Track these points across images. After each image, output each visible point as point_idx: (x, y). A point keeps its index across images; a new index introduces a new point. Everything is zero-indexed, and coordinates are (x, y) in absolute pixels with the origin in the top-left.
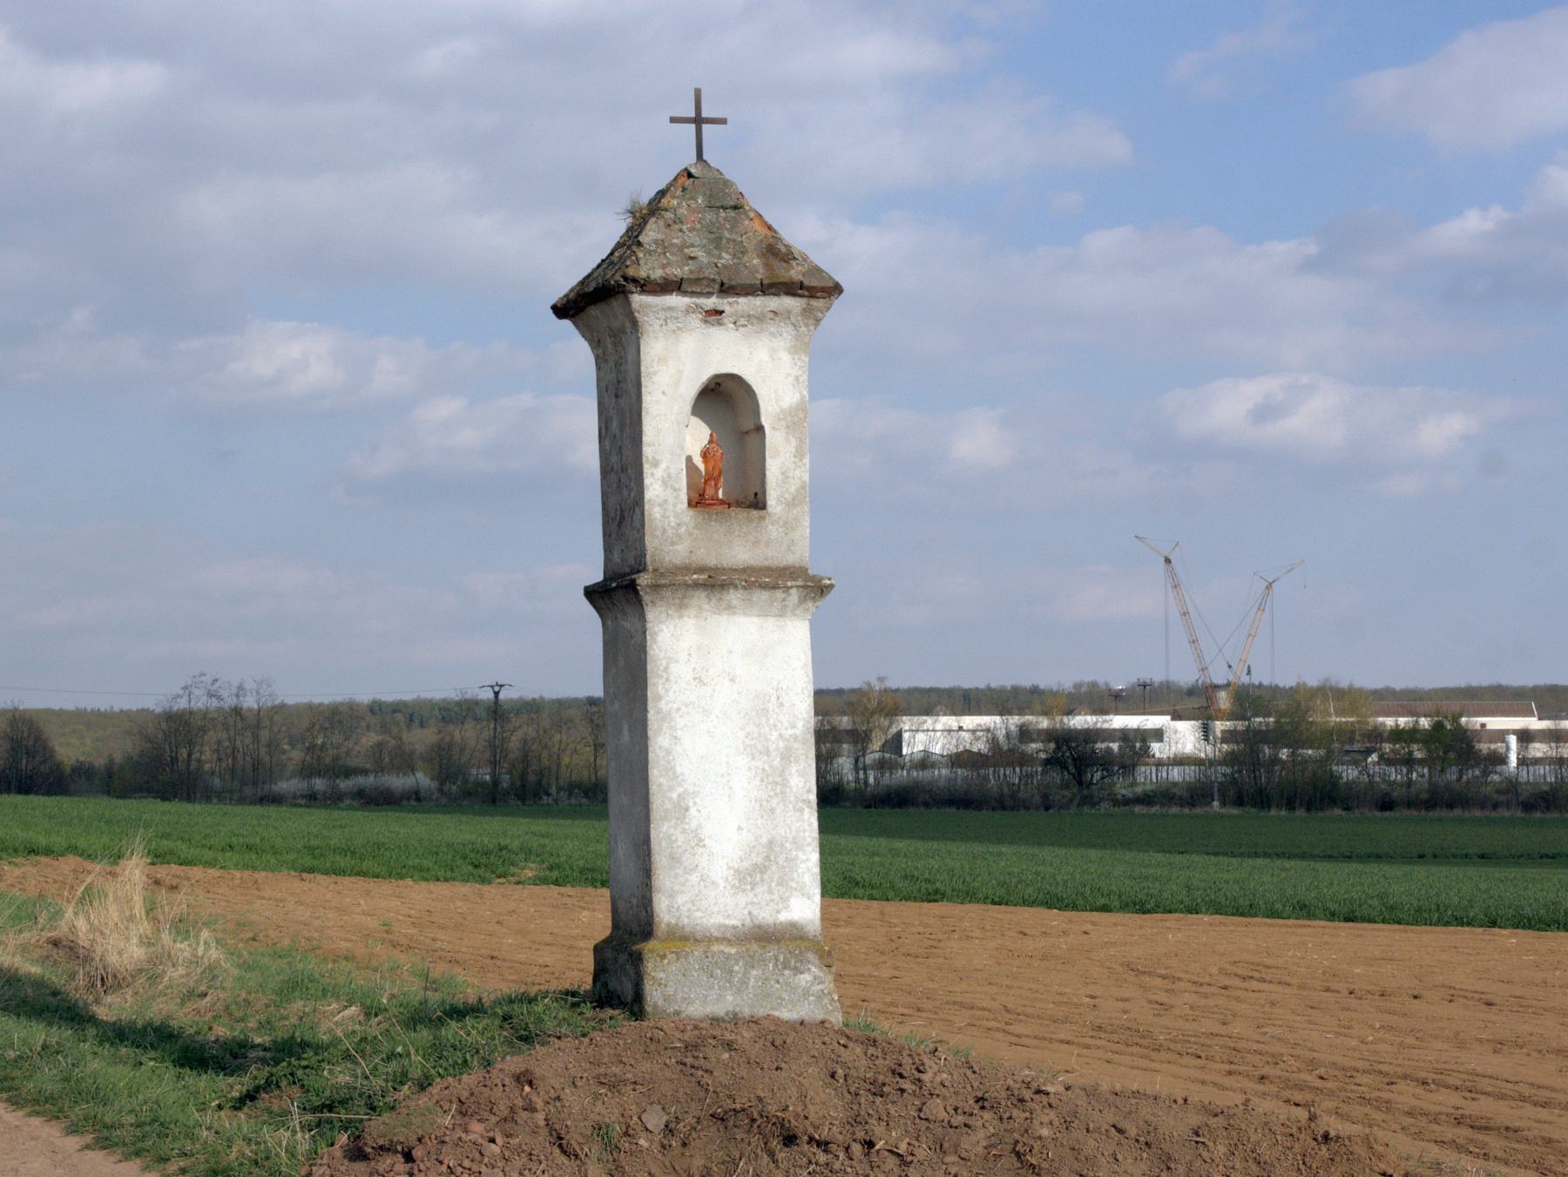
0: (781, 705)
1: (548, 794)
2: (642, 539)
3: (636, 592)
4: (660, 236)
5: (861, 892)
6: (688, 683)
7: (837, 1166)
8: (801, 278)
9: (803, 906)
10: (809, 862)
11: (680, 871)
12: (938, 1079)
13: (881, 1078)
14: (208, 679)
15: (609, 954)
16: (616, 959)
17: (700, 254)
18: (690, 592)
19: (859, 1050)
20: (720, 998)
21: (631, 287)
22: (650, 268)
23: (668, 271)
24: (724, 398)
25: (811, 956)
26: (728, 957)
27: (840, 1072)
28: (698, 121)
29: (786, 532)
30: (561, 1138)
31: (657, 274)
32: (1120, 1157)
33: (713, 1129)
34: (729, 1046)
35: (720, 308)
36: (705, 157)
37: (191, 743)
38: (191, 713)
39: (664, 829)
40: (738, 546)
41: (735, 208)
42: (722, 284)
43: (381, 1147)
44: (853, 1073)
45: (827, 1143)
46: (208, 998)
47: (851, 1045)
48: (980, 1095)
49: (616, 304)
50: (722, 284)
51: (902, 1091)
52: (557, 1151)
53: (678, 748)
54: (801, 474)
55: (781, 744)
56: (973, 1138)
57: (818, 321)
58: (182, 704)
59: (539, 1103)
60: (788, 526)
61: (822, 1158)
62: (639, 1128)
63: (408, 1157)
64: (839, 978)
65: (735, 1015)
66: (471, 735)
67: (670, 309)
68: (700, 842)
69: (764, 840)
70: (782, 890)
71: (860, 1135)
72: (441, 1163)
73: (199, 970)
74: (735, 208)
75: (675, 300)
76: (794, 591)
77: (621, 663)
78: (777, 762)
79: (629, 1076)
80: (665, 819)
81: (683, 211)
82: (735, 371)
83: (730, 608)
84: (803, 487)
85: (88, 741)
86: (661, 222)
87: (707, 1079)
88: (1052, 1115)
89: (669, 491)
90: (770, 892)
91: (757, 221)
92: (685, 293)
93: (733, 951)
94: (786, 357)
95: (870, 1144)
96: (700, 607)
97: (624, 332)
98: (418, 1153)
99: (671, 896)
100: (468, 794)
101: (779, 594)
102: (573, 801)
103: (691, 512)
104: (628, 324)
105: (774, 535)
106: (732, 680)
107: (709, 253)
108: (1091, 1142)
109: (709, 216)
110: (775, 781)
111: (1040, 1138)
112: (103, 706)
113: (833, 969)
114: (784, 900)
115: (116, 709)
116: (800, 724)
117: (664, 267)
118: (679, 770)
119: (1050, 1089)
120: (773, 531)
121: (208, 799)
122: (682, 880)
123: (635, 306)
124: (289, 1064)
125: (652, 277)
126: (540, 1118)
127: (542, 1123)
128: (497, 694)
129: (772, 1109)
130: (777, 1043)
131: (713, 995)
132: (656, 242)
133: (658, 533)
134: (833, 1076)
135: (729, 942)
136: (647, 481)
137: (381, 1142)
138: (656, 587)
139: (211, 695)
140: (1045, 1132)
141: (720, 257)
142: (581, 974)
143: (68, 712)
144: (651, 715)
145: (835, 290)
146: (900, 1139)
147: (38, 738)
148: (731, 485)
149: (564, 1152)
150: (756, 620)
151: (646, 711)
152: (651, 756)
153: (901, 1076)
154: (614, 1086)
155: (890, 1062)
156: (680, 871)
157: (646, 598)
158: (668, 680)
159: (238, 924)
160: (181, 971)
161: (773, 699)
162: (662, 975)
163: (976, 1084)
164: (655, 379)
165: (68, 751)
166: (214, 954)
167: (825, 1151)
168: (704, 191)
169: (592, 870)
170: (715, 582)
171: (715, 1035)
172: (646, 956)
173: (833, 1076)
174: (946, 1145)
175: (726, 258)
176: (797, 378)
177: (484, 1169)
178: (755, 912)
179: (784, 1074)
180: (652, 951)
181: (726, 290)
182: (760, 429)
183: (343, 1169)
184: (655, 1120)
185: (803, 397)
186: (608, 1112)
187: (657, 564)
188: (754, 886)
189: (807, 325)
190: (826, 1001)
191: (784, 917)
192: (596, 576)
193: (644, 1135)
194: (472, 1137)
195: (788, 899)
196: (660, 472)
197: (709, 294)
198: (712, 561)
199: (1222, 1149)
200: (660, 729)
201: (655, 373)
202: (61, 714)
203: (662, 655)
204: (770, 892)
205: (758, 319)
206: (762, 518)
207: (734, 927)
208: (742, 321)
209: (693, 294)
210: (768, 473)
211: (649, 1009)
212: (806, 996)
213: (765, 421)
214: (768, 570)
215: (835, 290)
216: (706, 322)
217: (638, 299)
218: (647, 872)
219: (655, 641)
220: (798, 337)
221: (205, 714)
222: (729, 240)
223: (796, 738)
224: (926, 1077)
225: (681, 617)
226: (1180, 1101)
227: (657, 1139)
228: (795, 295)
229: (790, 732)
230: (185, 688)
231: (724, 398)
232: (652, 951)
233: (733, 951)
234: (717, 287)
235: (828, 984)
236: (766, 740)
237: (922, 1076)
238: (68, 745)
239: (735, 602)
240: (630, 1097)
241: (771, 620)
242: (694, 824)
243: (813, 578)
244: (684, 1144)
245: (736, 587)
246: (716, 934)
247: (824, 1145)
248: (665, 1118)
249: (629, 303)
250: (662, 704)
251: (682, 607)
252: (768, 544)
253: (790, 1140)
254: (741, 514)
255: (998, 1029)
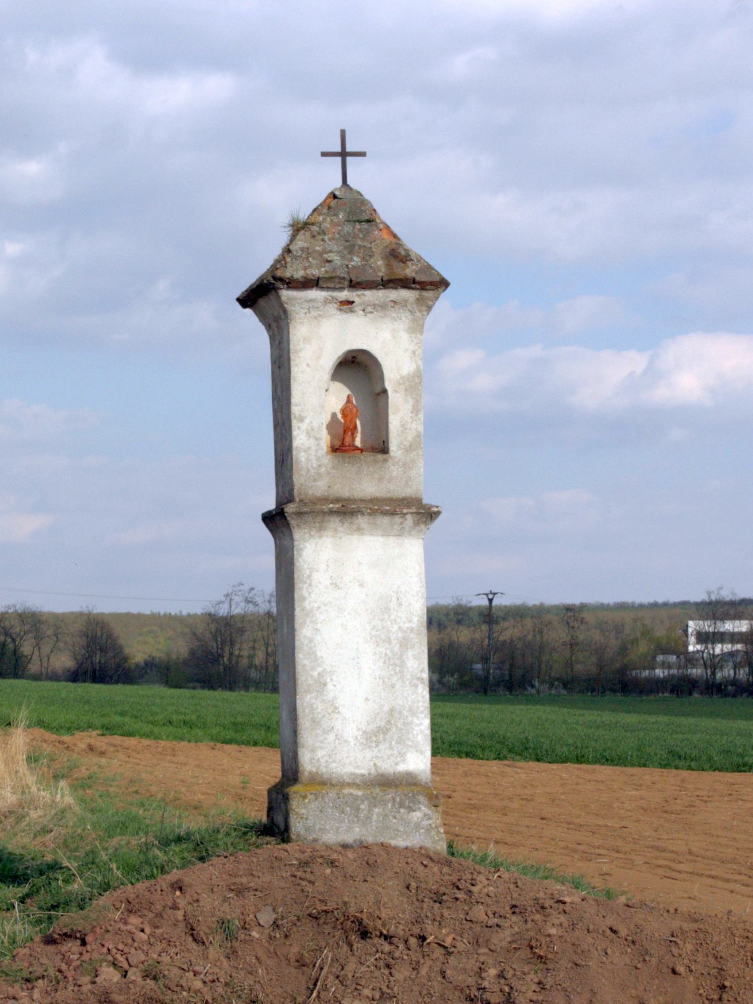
0: (400, 604)
1: (533, 686)
2: (291, 478)
3: (285, 518)
4: (305, 245)
5: (682, 763)
6: (326, 587)
7: (397, 954)
8: (413, 275)
9: (418, 760)
10: (421, 727)
11: (319, 732)
12: (486, 890)
13: (443, 889)
14: (246, 588)
15: (274, 796)
16: (277, 799)
17: (336, 259)
18: (327, 518)
19: (436, 869)
20: (350, 829)
21: (279, 284)
22: (295, 271)
23: (308, 272)
24: (356, 366)
25: (421, 798)
26: (356, 798)
27: (413, 884)
28: (344, 154)
29: (408, 468)
30: (193, 929)
31: (299, 274)
32: (609, 951)
33: (308, 926)
34: (332, 863)
35: (351, 299)
36: (349, 182)
37: (232, 643)
38: (232, 616)
39: (307, 699)
40: (365, 483)
41: (368, 221)
42: (351, 281)
43: (65, 934)
44: (423, 885)
45: (391, 937)
46: (52, 834)
47: (431, 864)
48: (514, 903)
49: (272, 296)
50: (351, 281)
51: (457, 899)
52: (190, 939)
53: (318, 638)
54: (417, 426)
55: (400, 635)
56: (501, 935)
57: (429, 308)
58: (223, 611)
59: (182, 903)
60: (407, 466)
61: (387, 948)
62: (253, 923)
63: (84, 943)
64: (445, 813)
65: (361, 842)
66: (558, 635)
67: (311, 300)
68: (336, 710)
69: (386, 709)
70: (400, 747)
71: (416, 930)
72: (103, 946)
73: (53, 812)
74: (368, 221)
75: (315, 294)
76: (409, 517)
77: (283, 572)
78: (397, 649)
79: (252, 885)
80: (308, 691)
81: (327, 225)
82: (364, 347)
83: (359, 530)
84: (418, 436)
85: (161, 640)
86: (308, 234)
87: (309, 889)
88: (563, 918)
89: (312, 441)
90: (391, 748)
91: (385, 231)
92: (322, 288)
93: (360, 793)
94: (404, 336)
95: (423, 938)
96: (336, 530)
97: (280, 318)
98: (89, 939)
99: (313, 751)
100: (463, 685)
101: (397, 519)
102: (553, 692)
103: (329, 457)
104: (282, 314)
105: (395, 473)
106: (362, 585)
107: (343, 257)
108: (591, 940)
109: (348, 228)
110: (395, 663)
111: (549, 936)
112: (173, 610)
113: (440, 809)
114: (402, 755)
115: (185, 613)
116: (415, 619)
117: (305, 269)
118: (319, 654)
119: (567, 899)
120: (394, 470)
121: (246, 688)
122: (321, 738)
123: (284, 299)
124: (48, 876)
125: (296, 276)
126: (180, 914)
127: (181, 918)
128: (491, 601)
129: (352, 910)
130: (371, 862)
131: (344, 827)
132: (302, 249)
133: (303, 472)
134: (408, 888)
135: (358, 786)
136: (295, 433)
137: (65, 931)
138: (299, 514)
139: (248, 601)
140: (553, 931)
141: (351, 260)
142: (258, 814)
143: (144, 615)
144: (298, 612)
145: (443, 284)
146: (447, 935)
147: (110, 636)
148: (361, 435)
149: (195, 940)
150: (381, 539)
151: (293, 609)
152: (297, 643)
153: (458, 888)
154: (240, 891)
155: (454, 878)
156: (319, 732)
157: (293, 523)
158: (310, 585)
159: (131, 781)
160: (40, 813)
161: (394, 599)
162: (304, 811)
163: (515, 896)
164: (301, 354)
165: (138, 651)
166: (69, 800)
167: (390, 943)
168: (348, 211)
169: (460, 743)
170: (346, 510)
171: (331, 858)
172: (292, 796)
173: (408, 888)
174: (481, 940)
175: (356, 260)
176: (414, 352)
177: (133, 951)
178: (379, 764)
179: (367, 884)
180: (296, 793)
181: (354, 285)
182: (385, 391)
183: (39, 950)
184: (266, 917)
185: (418, 367)
186: (232, 912)
187: (302, 497)
188: (378, 743)
189: (420, 311)
190: (433, 833)
191: (402, 768)
192: (270, 504)
193: (257, 928)
194: (129, 927)
195: (405, 754)
196: (304, 426)
197: (342, 289)
198: (345, 493)
199: (689, 947)
200: (305, 622)
201: (301, 350)
202: (138, 617)
203: (306, 566)
204: (391, 748)
205: (381, 307)
206: (386, 460)
207: (362, 775)
208: (369, 309)
209: (328, 289)
210: (390, 426)
211: (293, 837)
212: (418, 829)
213: (388, 385)
214: (390, 501)
215: (443, 284)
216: (341, 310)
217: (286, 294)
218: (295, 732)
219: (300, 556)
220: (415, 320)
221: (243, 617)
222: (360, 246)
223: (412, 630)
224: (475, 889)
225: (321, 537)
226: (672, 911)
227: (267, 931)
228: (409, 288)
229: (407, 625)
230: (227, 595)
231: (356, 366)
232: (296, 793)
233: (360, 793)
234: (346, 283)
235: (436, 819)
236: (389, 631)
237: (474, 889)
238: (145, 643)
239: (362, 525)
240: (250, 899)
241: (392, 539)
242: (331, 696)
243: (425, 507)
244: (286, 936)
245: (363, 514)
246: (348, 780)
247: (387, 938)
248: (275, 916)
249: (279, 297)
250: (306, 604)
251: (321, 529)
252: (389, 481)
253: (364, 934)
254: (369, 457)
255: (666, 866)
